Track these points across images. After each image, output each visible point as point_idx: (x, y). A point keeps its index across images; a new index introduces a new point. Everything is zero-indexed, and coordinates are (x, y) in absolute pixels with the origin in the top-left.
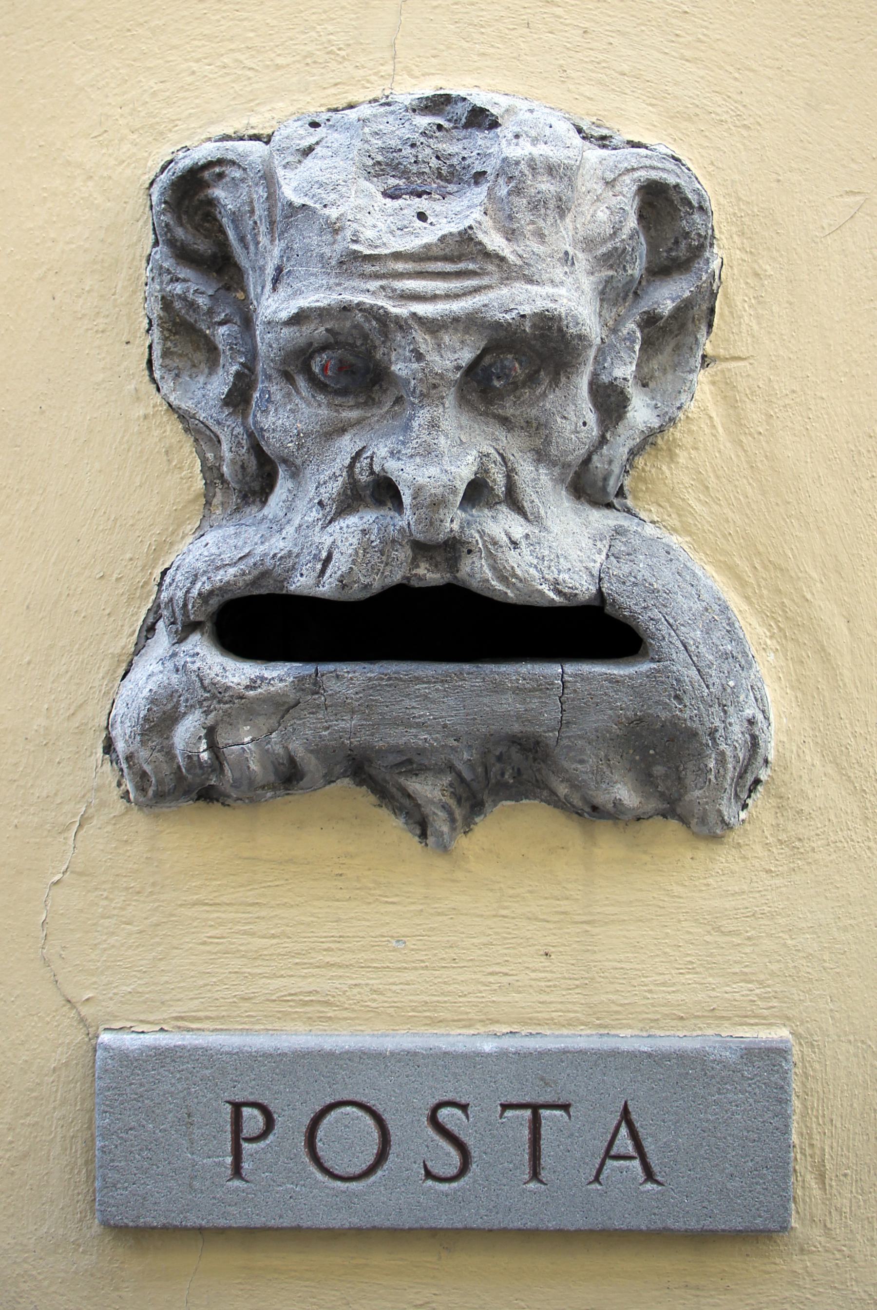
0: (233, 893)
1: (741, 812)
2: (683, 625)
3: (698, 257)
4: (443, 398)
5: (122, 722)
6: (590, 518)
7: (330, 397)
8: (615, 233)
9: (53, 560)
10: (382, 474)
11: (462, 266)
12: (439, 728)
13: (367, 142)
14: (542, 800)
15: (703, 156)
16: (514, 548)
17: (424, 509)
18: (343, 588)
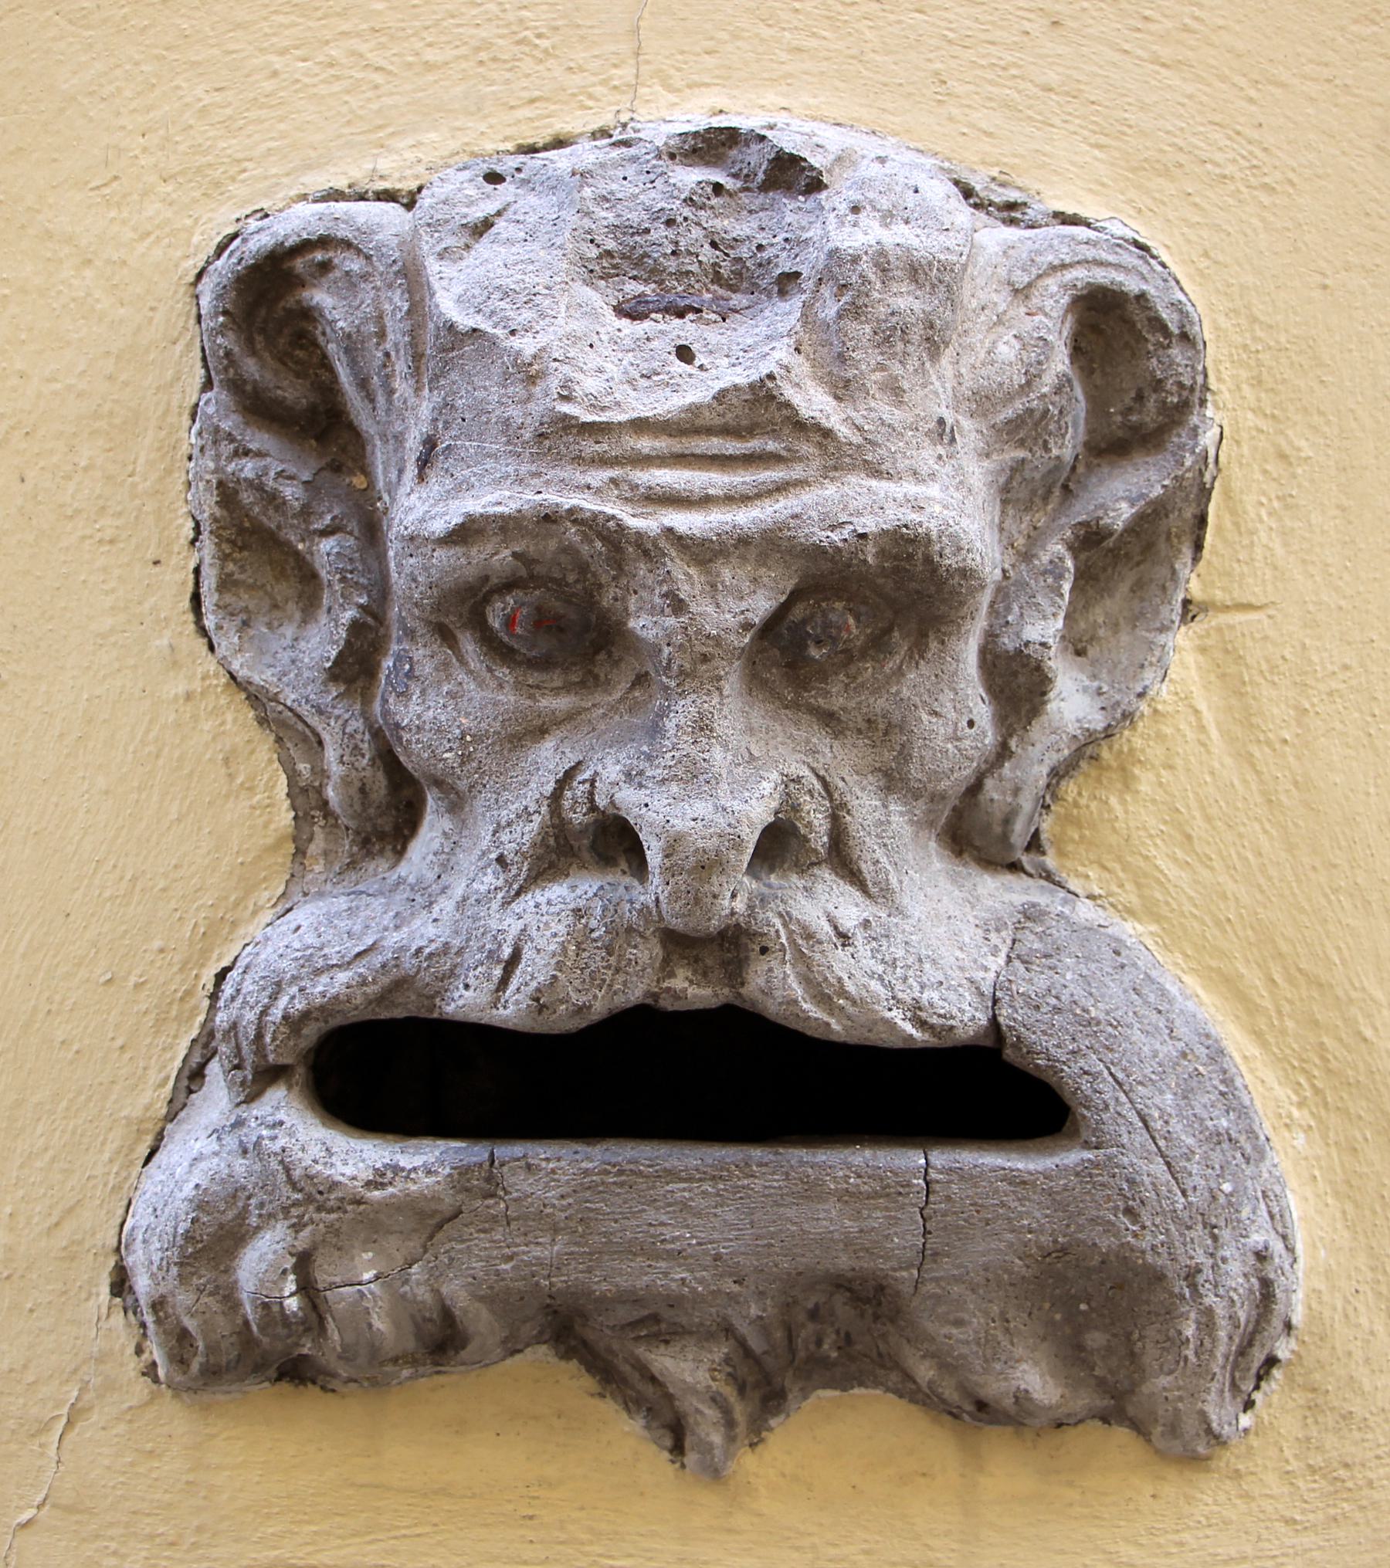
0: (340, 1547)
1: (1242, 1416)
2: (1140, 1083)
3: (1180, 423)
4: (719, 678)
5: (145, 1241)
6: (980, 890)
7: (519, 671)
8: (1029, 383)
9: (21, 950)
10: (611, 811)
11: (754, 445)
12: (708, 1261)
13: (587, 214)
14: (888, 1390)
15: (1189, 241)
16: (844, 945)
17: (685, 876)
18: (540, 1012)
